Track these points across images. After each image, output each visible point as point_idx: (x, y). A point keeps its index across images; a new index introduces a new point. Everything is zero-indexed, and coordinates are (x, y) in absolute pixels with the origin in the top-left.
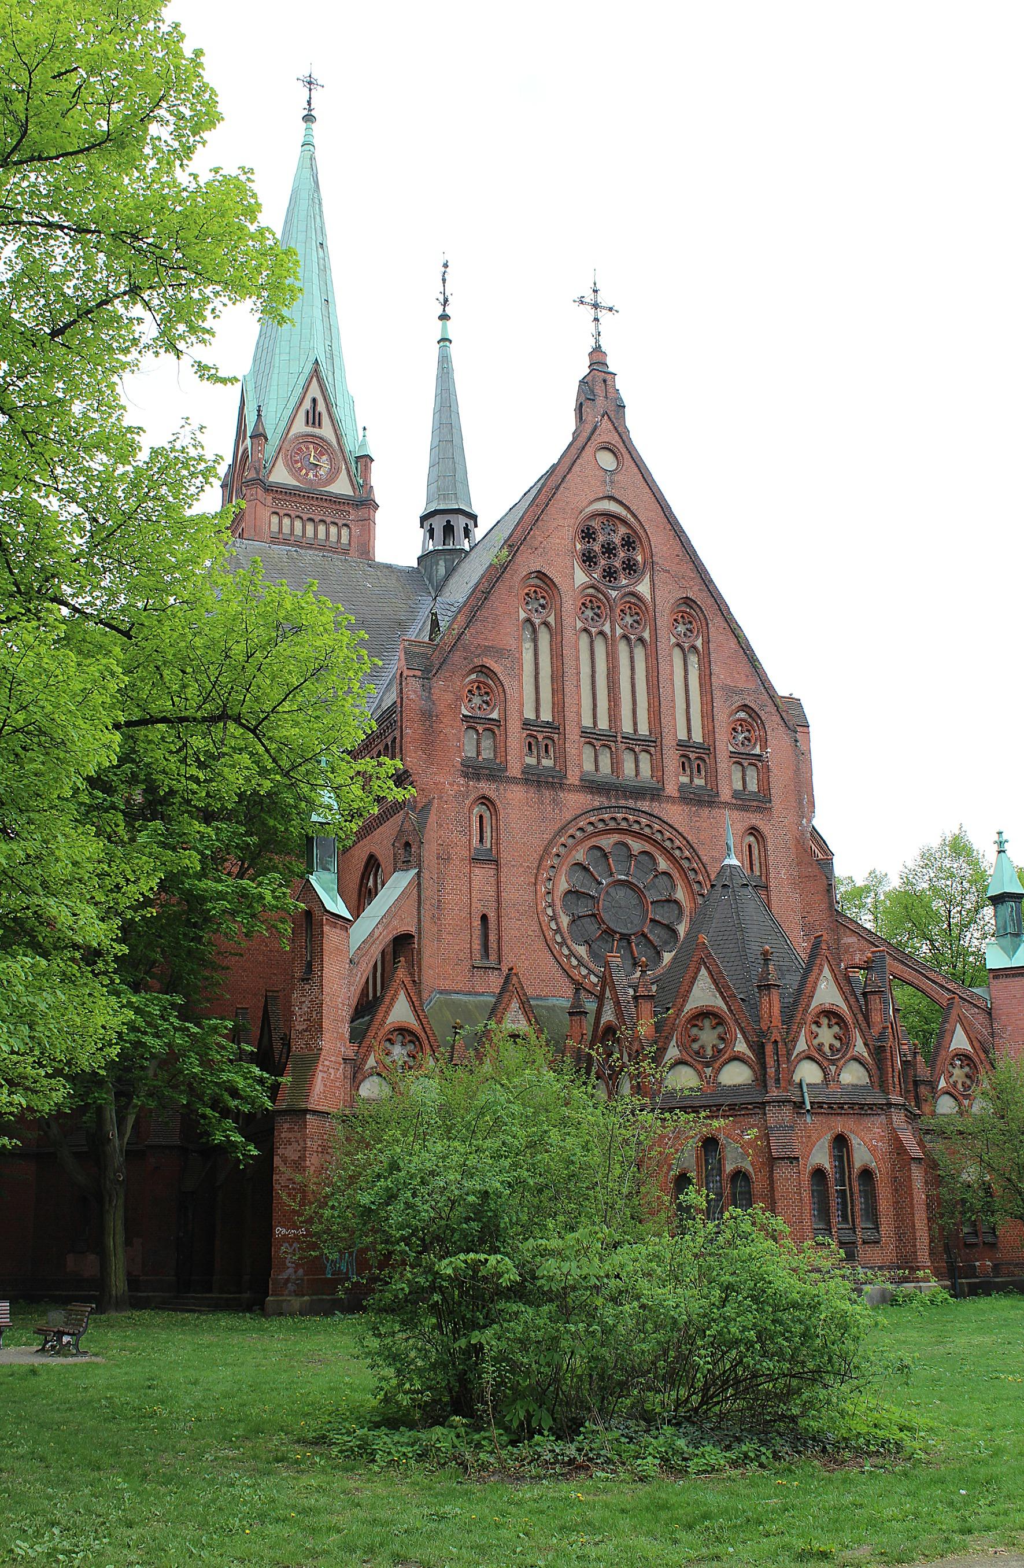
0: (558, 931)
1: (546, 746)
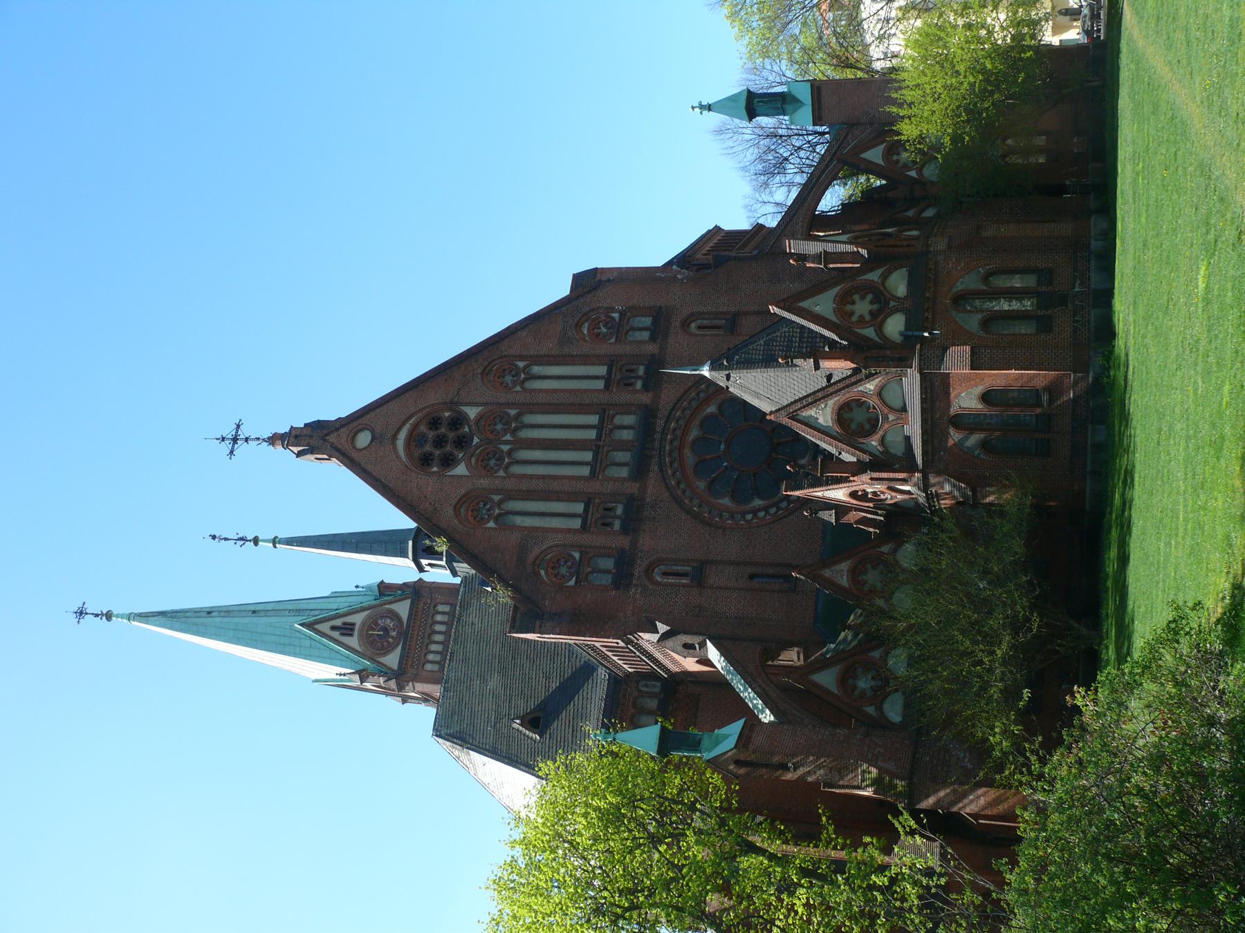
0: (766, 509)
1: (606, 509)
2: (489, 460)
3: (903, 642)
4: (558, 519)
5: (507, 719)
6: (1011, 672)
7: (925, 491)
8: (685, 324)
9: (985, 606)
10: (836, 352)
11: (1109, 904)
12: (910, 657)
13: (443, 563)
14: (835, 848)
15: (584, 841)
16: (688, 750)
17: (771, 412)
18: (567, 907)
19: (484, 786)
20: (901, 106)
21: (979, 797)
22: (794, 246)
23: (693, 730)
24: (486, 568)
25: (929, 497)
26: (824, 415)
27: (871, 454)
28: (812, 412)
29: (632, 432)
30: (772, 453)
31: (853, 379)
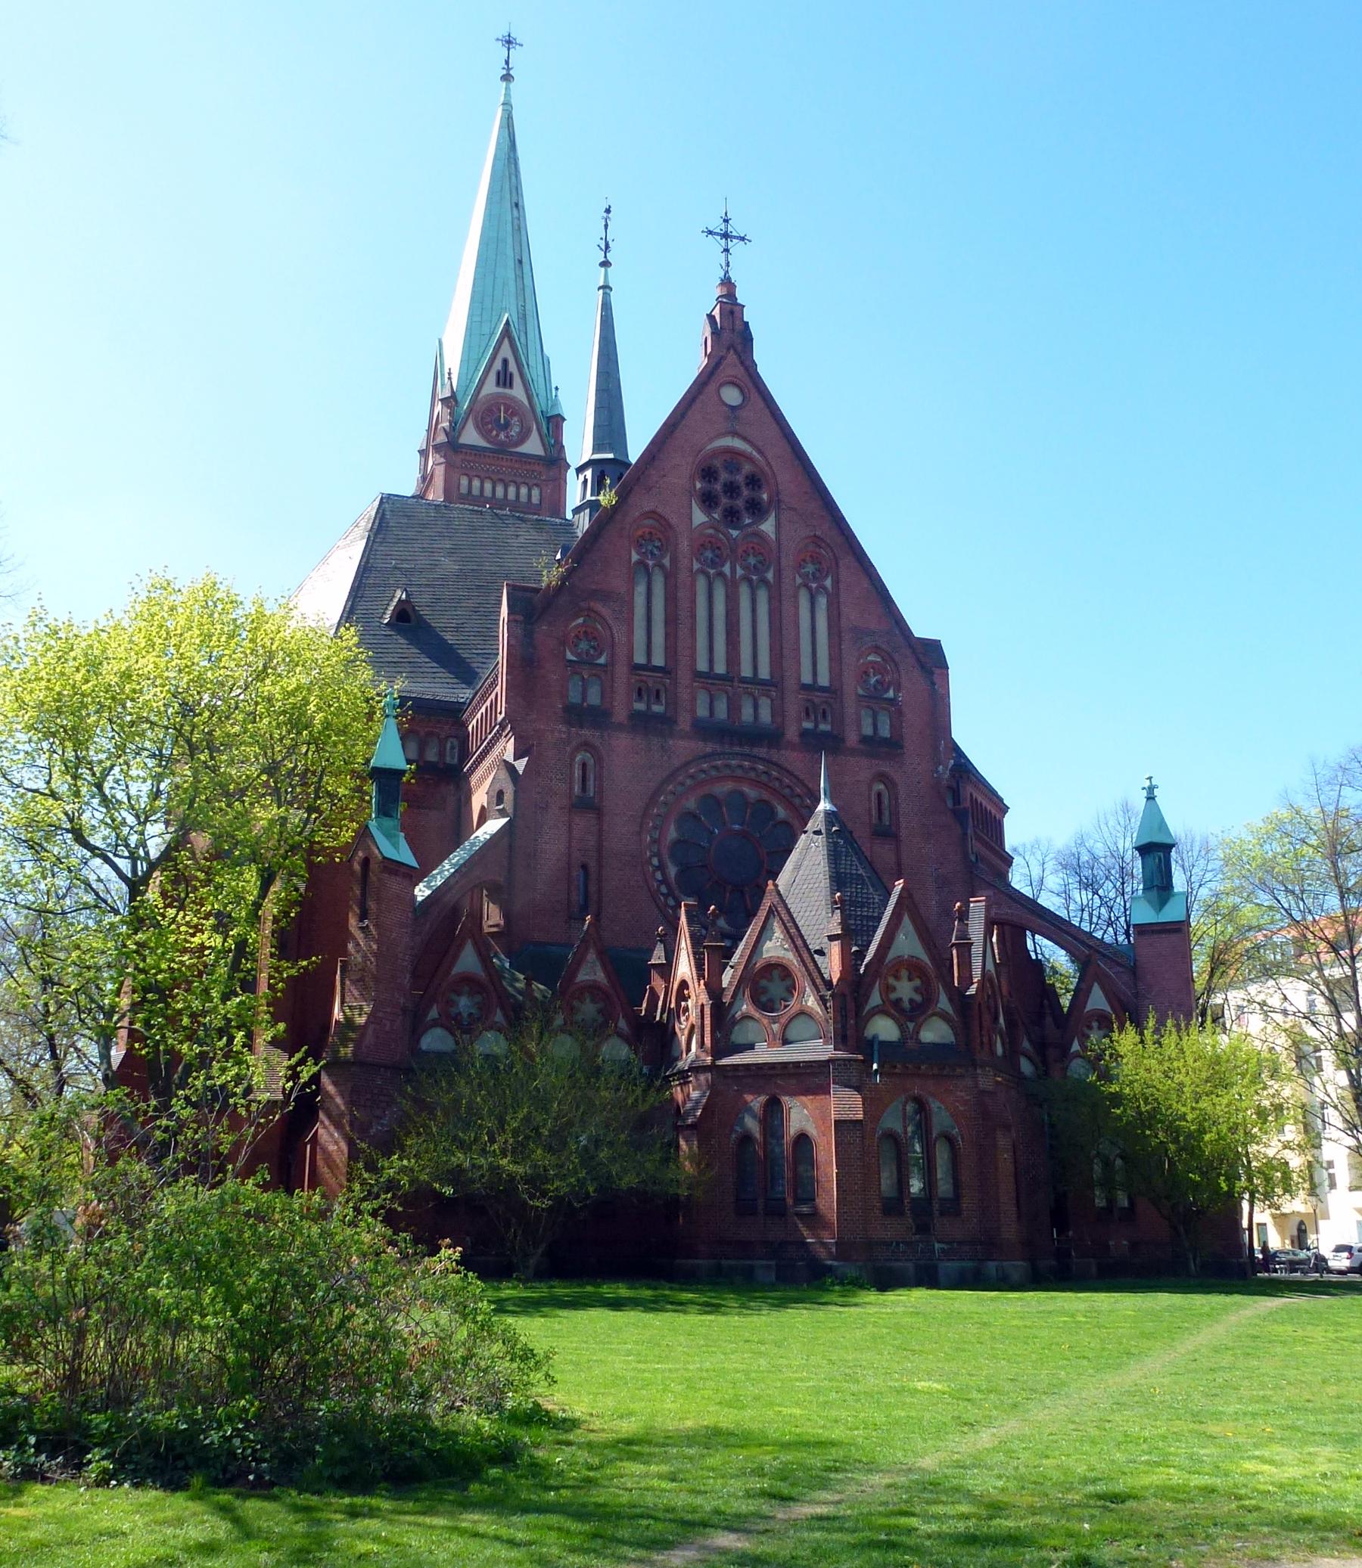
0: (665, 881)
1: (658, 692)
2: (711, 551)
3: (514, 1048)
4: (645, 639)
5: (400, 602)
6: (483, 1176)
7: (690, 1069)
8: (882, 777)
9: (557, 1143)
10: (851, 961)
11: (227, 1290)
12: (496, 1057)
13: (589, 497)
14: (271, 977)
15: (267, 687)
16: (378, 803)
17: (776, 886)
18: (189, 673)
19: (325, 559)
20: (1156, 1031)
21: (336, 1143)
22: (978, 907)
23: (402, 807)
24: (584, 553)
25: (683, 1075)
26: (776, 947)
27: (731, 1004)
28: (778, 933)
29: (751, 719)
30: (731, 887)
31: (818, 981)
